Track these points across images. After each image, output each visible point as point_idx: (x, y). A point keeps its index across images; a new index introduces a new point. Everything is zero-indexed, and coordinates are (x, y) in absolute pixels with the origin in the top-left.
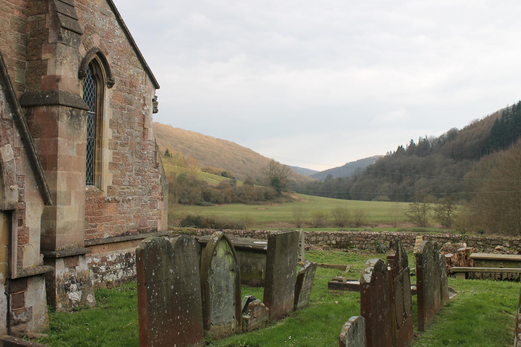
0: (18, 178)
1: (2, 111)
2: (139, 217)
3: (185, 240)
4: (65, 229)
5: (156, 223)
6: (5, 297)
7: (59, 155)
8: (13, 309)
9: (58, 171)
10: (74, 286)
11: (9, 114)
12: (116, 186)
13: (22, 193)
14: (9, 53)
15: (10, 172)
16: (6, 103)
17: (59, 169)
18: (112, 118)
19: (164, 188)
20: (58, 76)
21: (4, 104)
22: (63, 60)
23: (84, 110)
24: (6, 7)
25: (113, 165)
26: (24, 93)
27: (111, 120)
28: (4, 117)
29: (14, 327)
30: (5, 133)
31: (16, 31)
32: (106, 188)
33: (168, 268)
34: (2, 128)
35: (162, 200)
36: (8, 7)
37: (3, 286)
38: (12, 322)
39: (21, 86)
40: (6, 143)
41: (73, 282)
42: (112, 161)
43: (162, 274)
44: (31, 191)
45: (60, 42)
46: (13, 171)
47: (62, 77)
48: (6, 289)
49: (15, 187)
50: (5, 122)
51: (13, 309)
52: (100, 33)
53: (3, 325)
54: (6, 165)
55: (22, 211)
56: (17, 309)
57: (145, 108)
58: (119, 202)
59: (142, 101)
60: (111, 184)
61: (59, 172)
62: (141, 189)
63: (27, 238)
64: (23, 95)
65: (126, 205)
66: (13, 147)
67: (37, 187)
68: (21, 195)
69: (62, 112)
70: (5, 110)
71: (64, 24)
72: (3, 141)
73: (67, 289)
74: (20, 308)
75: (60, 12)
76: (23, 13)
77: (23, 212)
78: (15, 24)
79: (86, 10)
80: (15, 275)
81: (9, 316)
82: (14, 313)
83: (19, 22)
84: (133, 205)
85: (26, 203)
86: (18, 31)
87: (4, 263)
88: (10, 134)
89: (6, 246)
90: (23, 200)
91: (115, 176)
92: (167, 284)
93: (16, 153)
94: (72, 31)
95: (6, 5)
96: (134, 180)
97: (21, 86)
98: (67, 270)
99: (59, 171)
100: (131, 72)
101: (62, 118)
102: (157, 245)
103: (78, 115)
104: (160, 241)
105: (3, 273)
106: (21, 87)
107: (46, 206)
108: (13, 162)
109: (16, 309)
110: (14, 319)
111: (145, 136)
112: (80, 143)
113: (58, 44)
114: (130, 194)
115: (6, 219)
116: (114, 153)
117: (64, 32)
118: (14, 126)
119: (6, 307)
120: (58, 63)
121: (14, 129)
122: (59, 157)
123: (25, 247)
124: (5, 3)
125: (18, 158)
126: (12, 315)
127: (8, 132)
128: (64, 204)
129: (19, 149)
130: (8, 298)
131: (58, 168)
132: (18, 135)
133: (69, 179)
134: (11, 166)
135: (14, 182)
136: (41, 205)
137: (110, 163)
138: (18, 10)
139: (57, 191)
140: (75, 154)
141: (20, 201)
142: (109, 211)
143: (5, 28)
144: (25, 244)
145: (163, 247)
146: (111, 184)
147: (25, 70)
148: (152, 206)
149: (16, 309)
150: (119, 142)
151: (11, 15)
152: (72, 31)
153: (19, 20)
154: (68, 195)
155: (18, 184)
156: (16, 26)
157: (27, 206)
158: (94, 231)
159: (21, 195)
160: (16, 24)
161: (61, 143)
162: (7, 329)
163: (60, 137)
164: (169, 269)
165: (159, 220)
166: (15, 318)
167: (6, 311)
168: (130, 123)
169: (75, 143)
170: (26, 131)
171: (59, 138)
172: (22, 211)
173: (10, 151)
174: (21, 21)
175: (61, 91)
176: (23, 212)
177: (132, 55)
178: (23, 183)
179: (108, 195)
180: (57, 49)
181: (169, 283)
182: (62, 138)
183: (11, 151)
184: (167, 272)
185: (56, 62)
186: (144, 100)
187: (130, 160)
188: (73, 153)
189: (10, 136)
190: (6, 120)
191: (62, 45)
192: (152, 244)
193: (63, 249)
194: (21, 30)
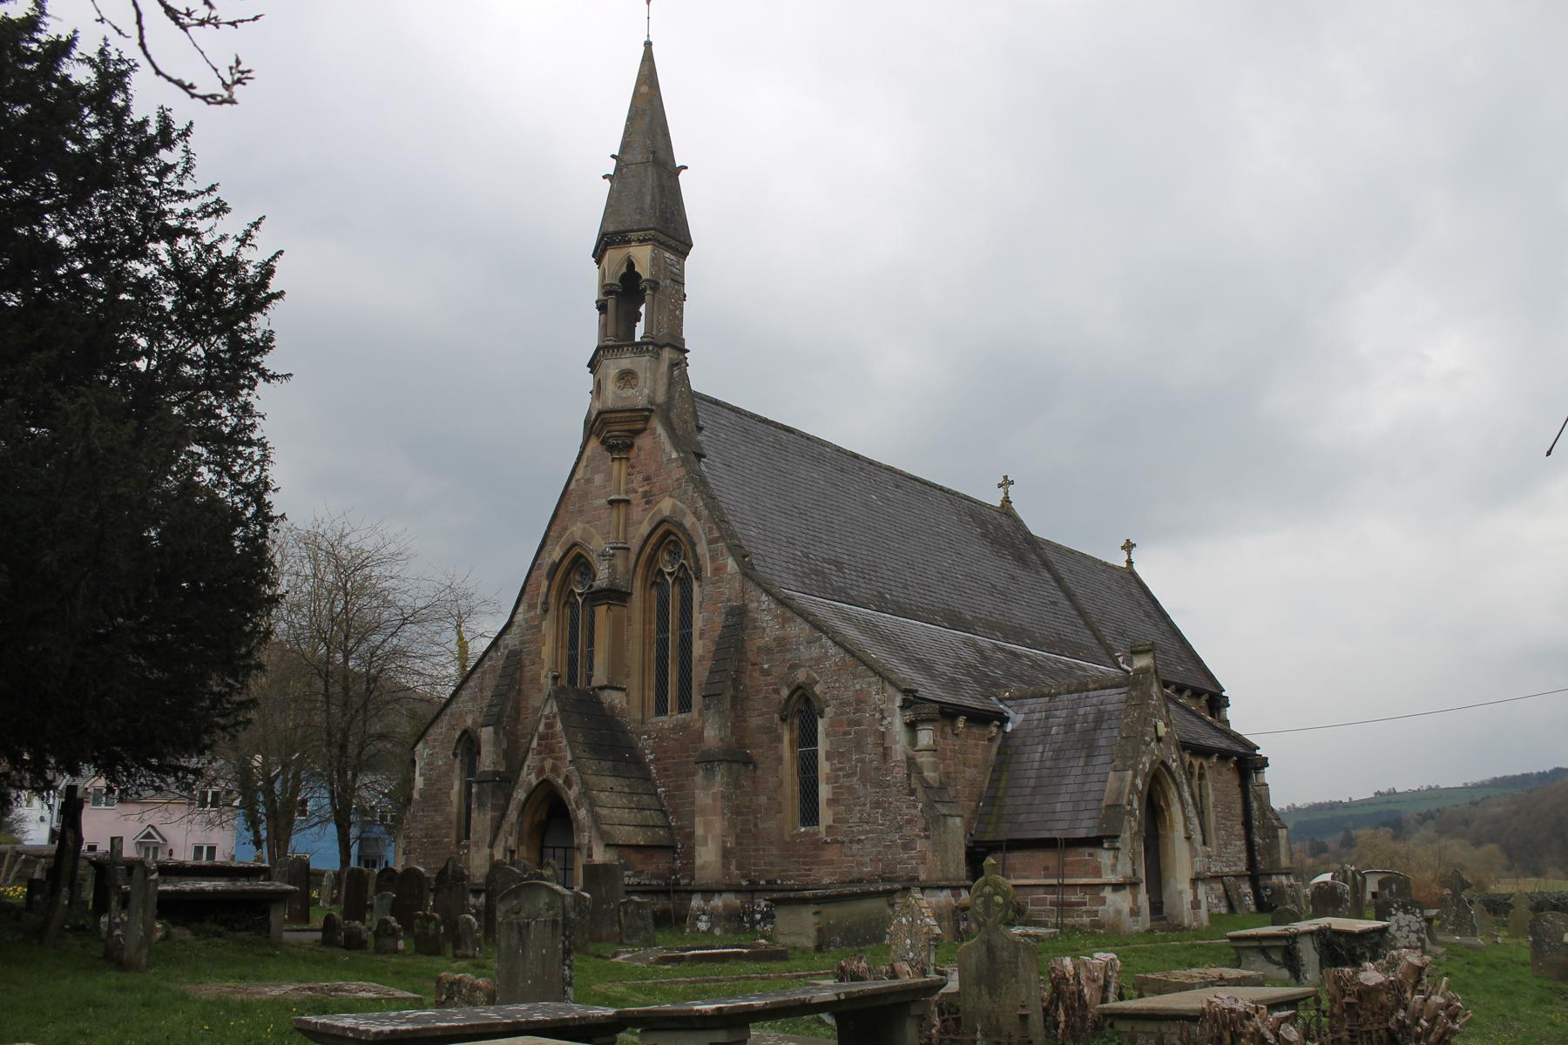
2: (880, 860)
4: (703, 867)
5: (915, 869)
10: (704, 918)
12: (838, 825)
18: (828, 749)
19: (930, 821)
23: (718, 761)
25: (832, 802)
27: (827, 752)
32: (824, 827)
35: (927, 837)
41: (704, 914)
42: (831, 797)
49: (586, 834)
52: (807, 665)
57: (885, 722)
58: (843, 843)
59: (878, 716)
60: (831, 823)
61: (696, 819)
62: (882, 825)
65: (855, 847)
73: (697, 918)
79: (788, 650)
84: (867, 846)
91: (835, 814)
94: (712, 695)
96: (869, 815)
98: (702, 902)
100: (858, 687)
103: (712, 767)
111: (888, 758)
112: (715, 791)
114: (862, 833)
116: (833, 788)
128: (702, 846)
133: (707, 825)
137: (828, 800)
140: (710, 802)
142: (829, 854)
146: (830, 822)
148: (907, 846)
150: (841, 773)
152: (712, 695)
154: (705, 839)
158: (809, 875)
165: (922, 866)
168: (859, 746)
169: (710, 792)
171: (696, 791)
177: (857, 666)
179: (827, 836)
186: (881, 714)
187: (861, 791)
188: (709, 801)
193: (702, 885)
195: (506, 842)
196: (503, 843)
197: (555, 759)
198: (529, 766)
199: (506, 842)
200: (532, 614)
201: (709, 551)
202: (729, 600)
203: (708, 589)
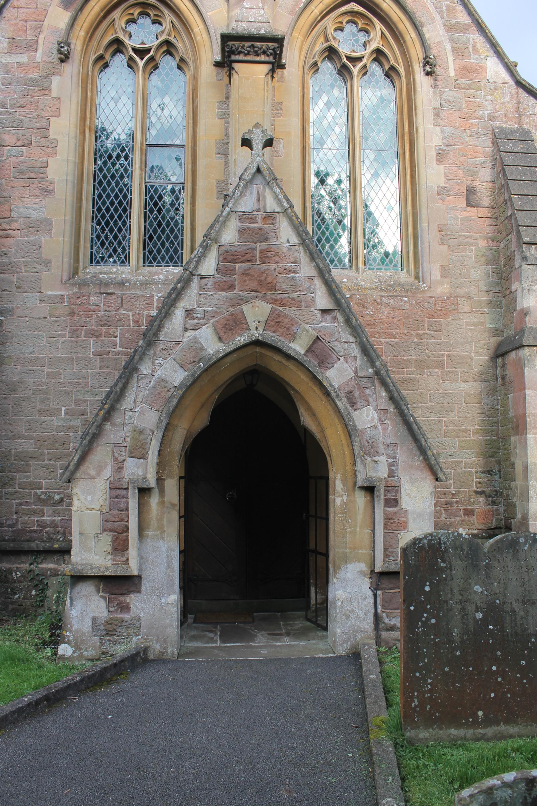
0: (386, 448)
1: (356, 367)
3: (522, 540)
6: (370, 593)
7: (529, 413)
8: (384, 610)
9: (528, 436)
11: (367, 370)
13: (394, 466)
14: (475, 293)
15: (372, 440)
16: (363, 357)
17: (530, 432)
20: (526, 308)
21: (358, 359)
22: (532, 285)
24: (466, 240)
26: (503, 338)
28: (359, 375)
29: (385, 633)
30: (362, 394)
31: (484, 265)
33: (470, 584)
34: (358, 388)
36: (469, 240)
37: (368, 580)
38: (381, 626)
39: (497, 330)
40: (365, 405)
43: (452, 591)
44: (410, 463)
45: (525, 263)
46: (377, 439)
47: (532, 309)
48: (371, 583)
50: (362, 379)
51: (384, 610)
53: (368, 627)
54: (366, 431)
55: (396, 488)
56: (390, 611)
63: (406, 523)
64: (501, 342)
66: (376, 409)
67: (421, 458)
68: (393, 468)
69: (530, 355)
70: (360, 366)
71: (528, 239)
72: (359, 403)
74: (396, 611)
75: (524, 225)
76: (493, 241)
77: (398, 490)
78: (482, 257)
80: (379, 568)
81: (377, 618)
82: (384, 615)
83: (488, 253)
85: (402, 478)
86: (487, 264)
87: (368, 551)
88: (371, 394)
89: (370, 531)
90: (396, 474)
92: (463, 609)
93: (381, 416)
95: (466, 238)
97: (497, 330)
99: (530, 435)
101: (531, 363)
102: (440, 543)
104: (448, 538)
105: (366, 563)
106: (498, 332)
107: (437, 482)
108: (376, 428)
109: (388, 611)
110: (384, 623)
113: (523, 267)
115: (369, 498)
117: (529, 249)
118: (377, 384)
119: (372, 605)
120: (524, 292)
121: (377, 387)
122: (529, 416)
123: (401, 534)
124: (464, 236)
125: (385, 422)
126: (382, 617)
127: (368, 391)
129: (386, 411)
130: (375, 596)
131: (528, 431)
132: (384, 394)
134: (374, 433)
135: (380, 452)
136: (428, 482)
138: (487, 238)
139: (527, 462)
141: (391, 474)
143: (467, 265)
144: (402, 530)
145: (455, 548)
147: (502, 310)
149: (388, 611)
151: (473, 248)
153: (487, 250)
155: (387, 455)
156: (484, 259)
157: (403, 482)
159: (393, 468)
160: (483, 256)
161: (531, 397)
162: (375, 633)
163: (529, 389)
164: (473, 584)
166: (387, 621)
167: (373, 611)
170: (391, 388)
172: (396, 488)
173: (371, 414)
174: (490, 251)
175: (530, 327)
176: (398, 490)
178: (396, 453)
180: (522, 273)
181: (471, 608)
182: (532, 389)
183: (372, 414)
184: (465, 590)
185: (522, 291)
189: (371, 396)
190: (364, 377)
191: (528, 266)
192: (426, 541)
194: (492, 261)
195: (119, 467)
196: (108, 472)
197: (274, 301)
198: (189, 312)
199: (119, 467)
200: (24, 58)
201: (451, 40)
202: (492, 118)
203: (450, 94)
